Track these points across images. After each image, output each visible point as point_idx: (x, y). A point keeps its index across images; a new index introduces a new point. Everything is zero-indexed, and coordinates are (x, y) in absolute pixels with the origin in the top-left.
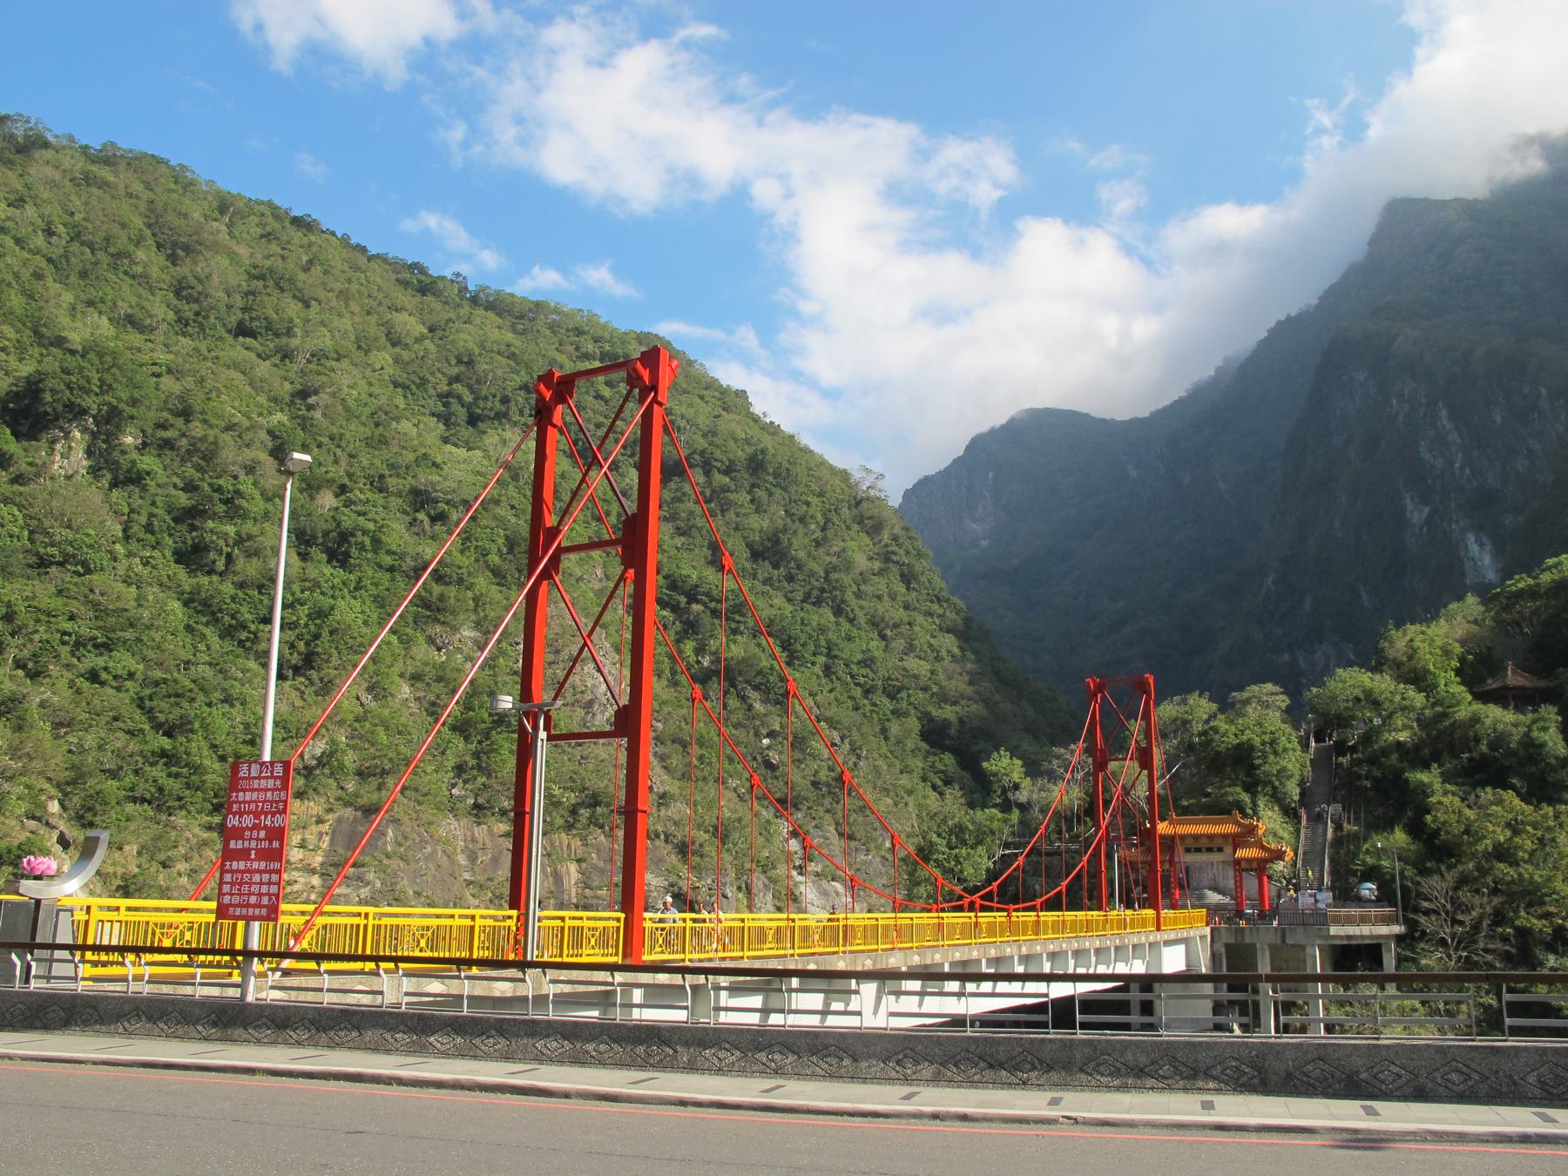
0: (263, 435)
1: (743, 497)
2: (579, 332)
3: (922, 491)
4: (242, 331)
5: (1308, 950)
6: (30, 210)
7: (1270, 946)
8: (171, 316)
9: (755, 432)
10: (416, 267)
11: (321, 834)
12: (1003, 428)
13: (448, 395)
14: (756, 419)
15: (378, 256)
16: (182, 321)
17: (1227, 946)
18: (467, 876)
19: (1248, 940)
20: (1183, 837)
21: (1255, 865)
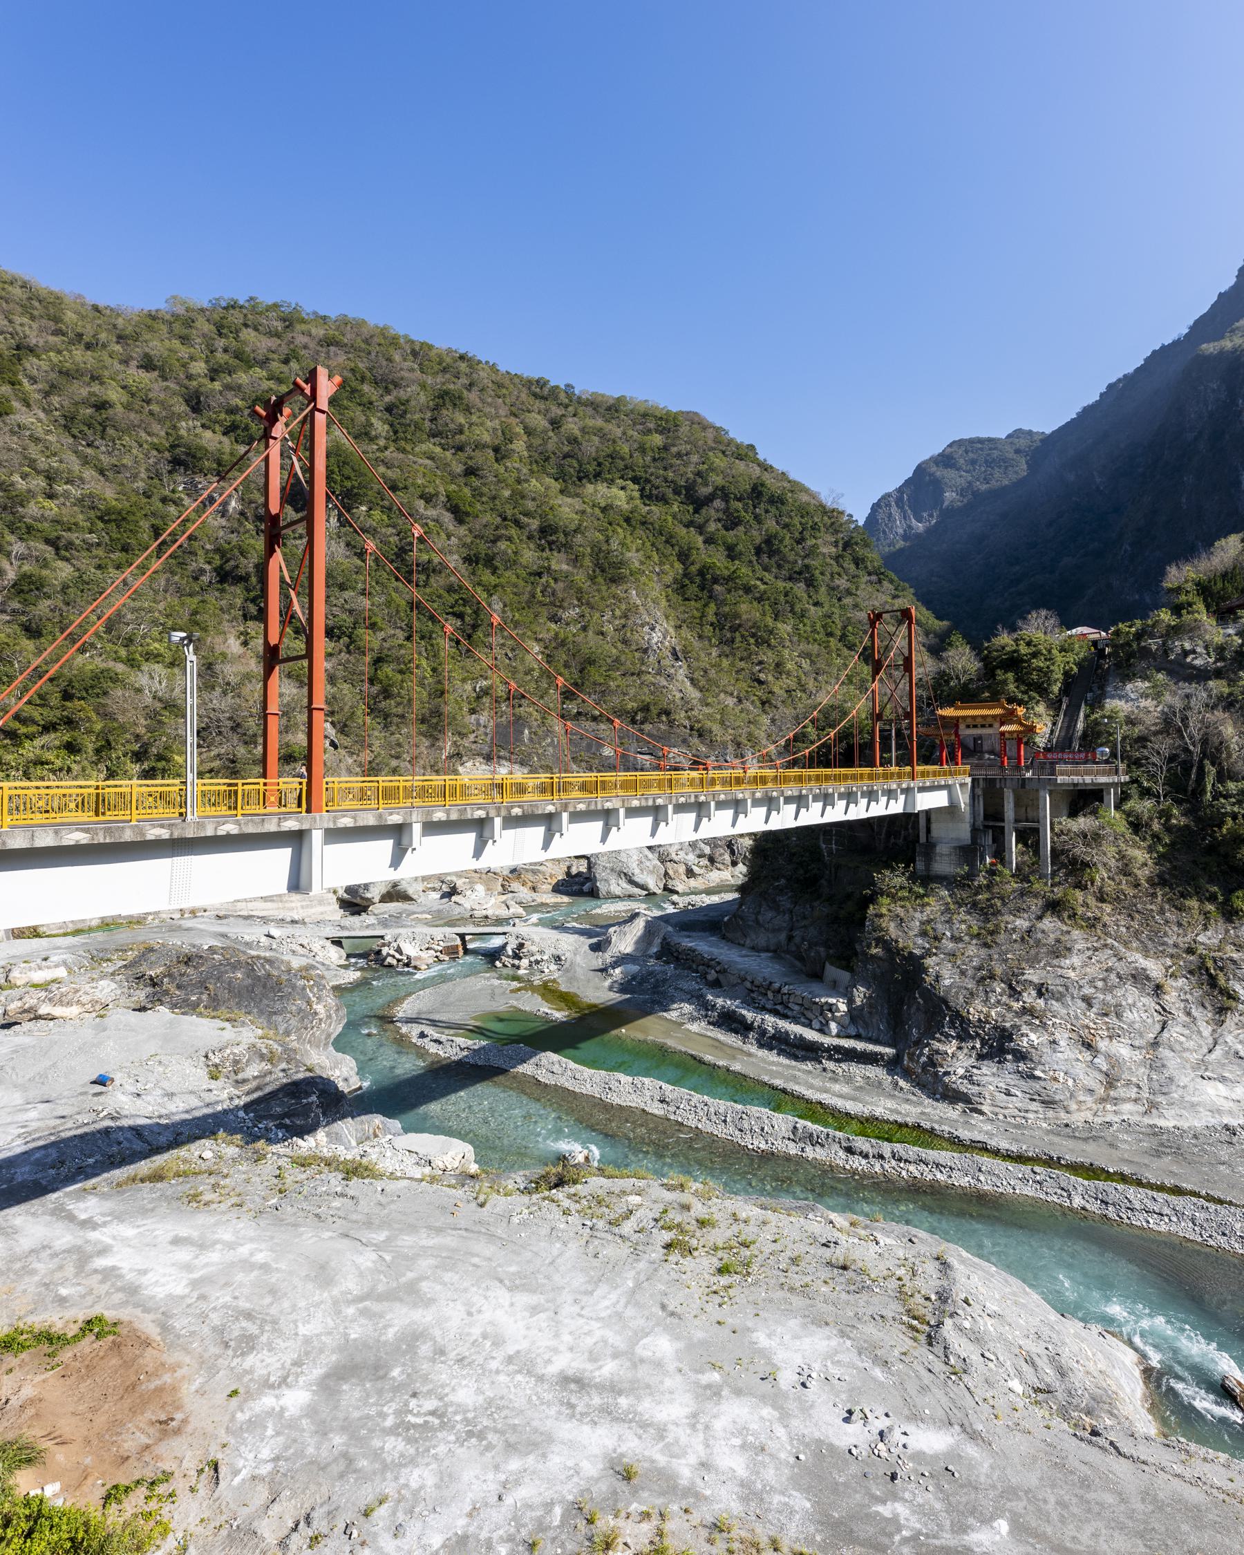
2: (645, 415)
5: (1041, 793)
10: (541, 383)
20: (964, 718)
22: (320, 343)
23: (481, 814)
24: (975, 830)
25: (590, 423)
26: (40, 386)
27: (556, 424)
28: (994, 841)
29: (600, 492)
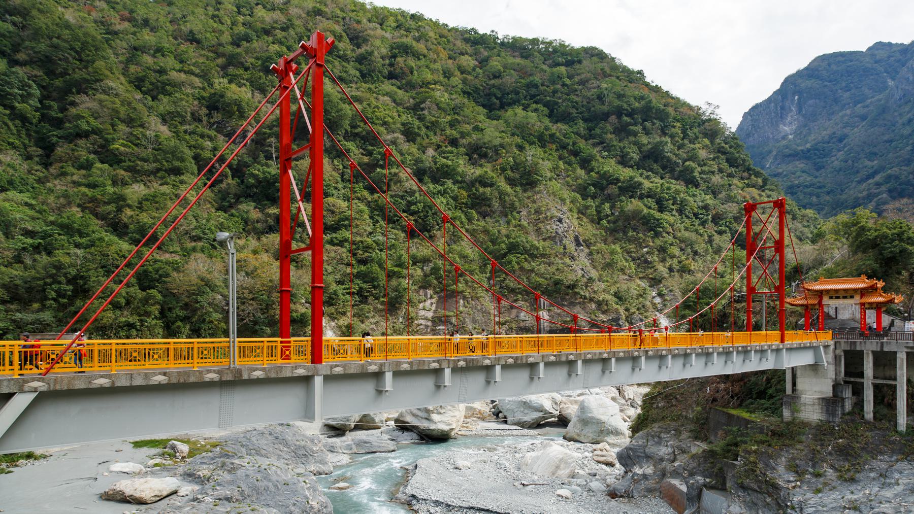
0: (399, 125)
1: (639, 128)
3: (755, 114)
4: (391, 76)
6: (291, 32)
7: (873, 352)
8: (358, 74)
9: (646, 92)
11: (432, 304)
12: (806, 69)
13: (489, 95)
14: (647, 85)
15: (453, 28)
16: (363, 76)
17: (845, 352)
18: (497, 319)
19: (858, 348)
20: (828, 291)
21: (874, 306)
22: (308, 13)
23: (435, 365)
24: (835, 387)
25: (511, 60)
26: (120, 59)
27: (483, 62)
28: (854, 393)
29: (517, 114)
